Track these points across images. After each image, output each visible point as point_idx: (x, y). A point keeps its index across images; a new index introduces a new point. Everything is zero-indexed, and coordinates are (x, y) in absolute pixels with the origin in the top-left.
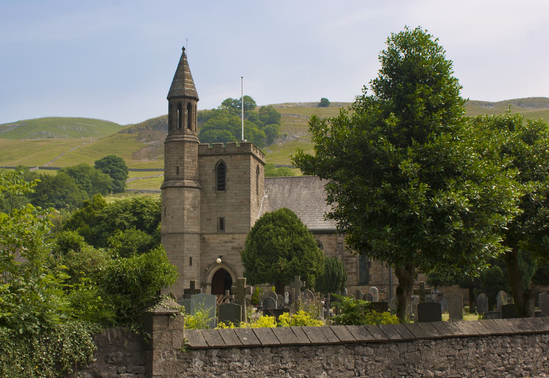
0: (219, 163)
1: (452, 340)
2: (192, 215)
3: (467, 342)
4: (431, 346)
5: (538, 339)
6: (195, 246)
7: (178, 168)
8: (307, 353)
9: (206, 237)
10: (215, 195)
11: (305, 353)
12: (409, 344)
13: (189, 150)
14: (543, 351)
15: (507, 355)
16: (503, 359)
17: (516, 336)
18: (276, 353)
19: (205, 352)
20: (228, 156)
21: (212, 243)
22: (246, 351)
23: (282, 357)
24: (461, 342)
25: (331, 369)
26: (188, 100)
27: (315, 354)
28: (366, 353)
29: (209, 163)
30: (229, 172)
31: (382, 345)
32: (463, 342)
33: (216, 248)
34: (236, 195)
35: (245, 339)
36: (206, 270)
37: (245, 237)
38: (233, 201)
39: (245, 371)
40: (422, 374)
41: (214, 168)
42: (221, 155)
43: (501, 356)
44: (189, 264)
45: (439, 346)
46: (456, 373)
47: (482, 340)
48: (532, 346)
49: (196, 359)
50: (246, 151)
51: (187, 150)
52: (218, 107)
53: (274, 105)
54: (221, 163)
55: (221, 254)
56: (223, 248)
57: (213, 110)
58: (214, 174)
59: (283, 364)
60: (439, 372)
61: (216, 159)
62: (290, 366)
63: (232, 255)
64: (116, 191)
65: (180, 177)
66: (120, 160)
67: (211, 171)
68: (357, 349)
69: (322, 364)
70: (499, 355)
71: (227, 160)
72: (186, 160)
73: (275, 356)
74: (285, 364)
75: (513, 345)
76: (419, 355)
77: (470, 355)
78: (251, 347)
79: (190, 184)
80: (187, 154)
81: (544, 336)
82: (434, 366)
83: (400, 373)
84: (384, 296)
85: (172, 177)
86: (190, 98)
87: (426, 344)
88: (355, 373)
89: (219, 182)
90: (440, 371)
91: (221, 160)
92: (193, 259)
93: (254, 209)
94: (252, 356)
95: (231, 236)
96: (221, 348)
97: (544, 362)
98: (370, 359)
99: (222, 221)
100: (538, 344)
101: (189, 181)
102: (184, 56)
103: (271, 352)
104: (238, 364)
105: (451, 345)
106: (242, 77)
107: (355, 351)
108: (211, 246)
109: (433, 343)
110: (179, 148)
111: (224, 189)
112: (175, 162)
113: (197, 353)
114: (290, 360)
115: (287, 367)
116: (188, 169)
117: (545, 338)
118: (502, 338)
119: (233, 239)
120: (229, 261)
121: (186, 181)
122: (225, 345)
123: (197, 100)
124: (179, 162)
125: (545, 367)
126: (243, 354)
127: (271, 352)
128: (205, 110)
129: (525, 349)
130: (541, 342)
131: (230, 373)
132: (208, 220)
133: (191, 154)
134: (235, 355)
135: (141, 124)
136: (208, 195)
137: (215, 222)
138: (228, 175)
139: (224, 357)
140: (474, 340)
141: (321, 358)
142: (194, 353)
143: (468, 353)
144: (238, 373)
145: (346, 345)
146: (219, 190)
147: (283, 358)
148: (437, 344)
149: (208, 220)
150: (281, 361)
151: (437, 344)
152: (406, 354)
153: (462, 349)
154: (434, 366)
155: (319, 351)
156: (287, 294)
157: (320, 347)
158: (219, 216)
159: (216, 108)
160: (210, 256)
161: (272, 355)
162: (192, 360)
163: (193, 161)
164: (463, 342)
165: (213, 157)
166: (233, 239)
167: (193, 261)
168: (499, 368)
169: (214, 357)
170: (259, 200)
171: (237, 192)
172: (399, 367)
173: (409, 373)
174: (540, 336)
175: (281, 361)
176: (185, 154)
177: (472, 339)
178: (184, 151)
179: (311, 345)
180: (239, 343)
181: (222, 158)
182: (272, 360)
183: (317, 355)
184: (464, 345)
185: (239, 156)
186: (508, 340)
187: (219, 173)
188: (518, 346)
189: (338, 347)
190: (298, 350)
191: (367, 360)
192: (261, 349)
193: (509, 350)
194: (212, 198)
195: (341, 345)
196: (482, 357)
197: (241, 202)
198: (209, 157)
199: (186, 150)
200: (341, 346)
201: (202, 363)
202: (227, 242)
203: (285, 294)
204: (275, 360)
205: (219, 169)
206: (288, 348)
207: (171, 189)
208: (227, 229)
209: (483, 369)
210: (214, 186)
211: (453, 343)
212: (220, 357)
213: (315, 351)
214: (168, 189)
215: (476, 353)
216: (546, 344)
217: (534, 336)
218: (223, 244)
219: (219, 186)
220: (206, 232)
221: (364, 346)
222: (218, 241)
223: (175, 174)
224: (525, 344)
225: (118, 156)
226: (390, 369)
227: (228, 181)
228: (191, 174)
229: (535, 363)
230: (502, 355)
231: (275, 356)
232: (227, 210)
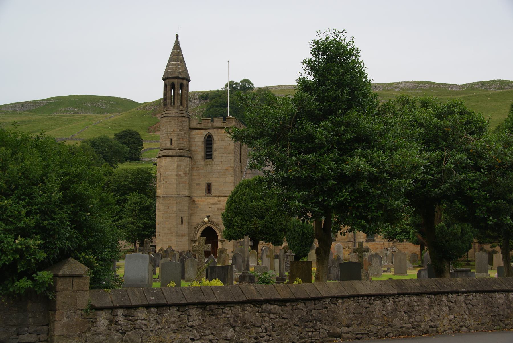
1: (359, 299)
3: (374, 301)
4: (338, 304)
5: (444, 298)
7: (171, 139)
8: (214, 311)
9: (196, 199)
10: (203, 163)
11: (212, 311)
12: (317, 302)
14: (450, 310)
15: (414, 313)
16: (410, 317)
17: (423, 295)
18: (183, 311)
19: (110, 311)
20: (215, 130)
22: (152, 309)
23: (189, 315)
24: (368, 300)
25: (238, 326)
27: (223, 312)
28: (272, 311)
29: (199, 136)
30: (216, 144)
31: (289, 303)
32: (370, 300)
33: (204, 209)
34: (221, 164)
35: (152, 298)
36: (195, 228)
37: (226, 199)
38: (219, 168)
39: (151, 329)
40: (328, 330)
42: (209, 129)
43: (408, 314)
44: (180, 223)
45: (346, 304)
46: (363, 329)
47: (389, 299)
48: (439, 304)
49: (101, 319)
52: (222, 88)
53: (269, 87)
54: (209, 135)
55: (208, 215)
56: (210, 209)
57: (218, 91)
58: (203, 145)
59: (190, 321)
60: (346, 328)
61: (205, 132)
62: (197, 323)
64: (132, 159)
66: (136, 133)
67: (201, 143)
68: (264, 307)
69: (229, 321)
70: (405, 313)
73: (181, 315)
74: (192, 321)
75: (419, 303)
76: (326, 313)
77: (376, 312)
78: (157, 306)
79: (182, 153)
81: (450, 295)
82: (341, 323)
83: (307, 329)
84: (349, 251)
85: (166, 147)
86: (183, 79)
87: (334, 302)
88: (262, 330)
89: (207, 152)
90: (347, 327)
92: (184, 218)
93: (238, 176)
94: (159, 314)
96: (127, 308)
97: (450, 320)
98: (278, 317)
99: (209, 186)
100: (445, 303)
102: (177, 42)
103: (178, 310)
104: (144, 322)
105: (358, 303)
106: (228, 61)
107: (262, 309)
109: (340, 301)
110: (173, 122)
112: (169, 135)
113: (102, 313)
114: (197, 318)
115: (194, 325)
117: (452, 297)
118: (409, 297)
120: (215, 221)
122: (130, 304)
123: (189, 80)
124: (172, 135)
125: (452, 324)
126: (149, 312)
127: (178, 310)
128: (210, 91)
129: (431, 307)
130: (447, 301)
131: (136, 331)
132: (197, 184)
133: (183, 128)
134: (141, 314)
135: (152, 102)
137: (204, 186)
138: (215, 146)
139: (130, 316)
140: (381, 298)
141: (228, 316)
142: (100, 312)
143: (375, 311)
144: (144, 331)
145: (253, 303)
146: (207, 159)
147: (190, 316)
148: (343, 302)
149: (197, 184)
150: (188, 319)
151: (343, 302)
152: (313, 311)
153: (369, 307)
154: (341, 323)
155: (227, 308)
157: (227, 305)
159: (220, 89)
160: (198, 216)
161: (179, 313)
162: (96, 319)
163: (185, 134)
164: (370, 300)
165: (202, 131)
167: (184, 221)
168: (405, 325)
169: (120, 316)
170: (243, 168)
171: (222, 160)
172: (306, 323)
173: (315, 330)
174: (447, 295)
175: (188, 319)
177: (379, 298)
179: (219, 304)
180: (145, 303)
181: (210, 131)
182: (179, 318)
183: (224, 313)
184: (371, 303)
186: (415, 298)
187: (207, 144)
188: (425, 305)
189: (246, 305)
190: (205, 309)
191: (274, 318)
192: (168, 307)
193: (416, 309)
194: (201, 166)
195: (249, 303)
196: (389, 315)
197: (226, 169)
198: (198, 131)
200: (249, 305)
201: (106, 322)
202: (213, 204)
204: (182, 317)
205: (207, 141)
206: (196, 307)
207: (164, 157)
208: (214, 192)
209: (390, 325)
210: (203, 155)
211: (360, 301)
212: (126, 316)
213: (222, 309)
214: (163, 158)
215: (383, 310)
216: (452, 302)
217: (441, 295)
218: (210, 206)
219: (207, 155)
220: (196, 195)
221: (271, 304)
222: (206, 203)
223: (169, 145)
224: (432, 303)
225: (134, 129)
226: (297, 326)
227: (215, 151)
228: (183, 145)
229: (442, 320)
230: (409, 313)
231: (181, 315)
232: (214, 176)
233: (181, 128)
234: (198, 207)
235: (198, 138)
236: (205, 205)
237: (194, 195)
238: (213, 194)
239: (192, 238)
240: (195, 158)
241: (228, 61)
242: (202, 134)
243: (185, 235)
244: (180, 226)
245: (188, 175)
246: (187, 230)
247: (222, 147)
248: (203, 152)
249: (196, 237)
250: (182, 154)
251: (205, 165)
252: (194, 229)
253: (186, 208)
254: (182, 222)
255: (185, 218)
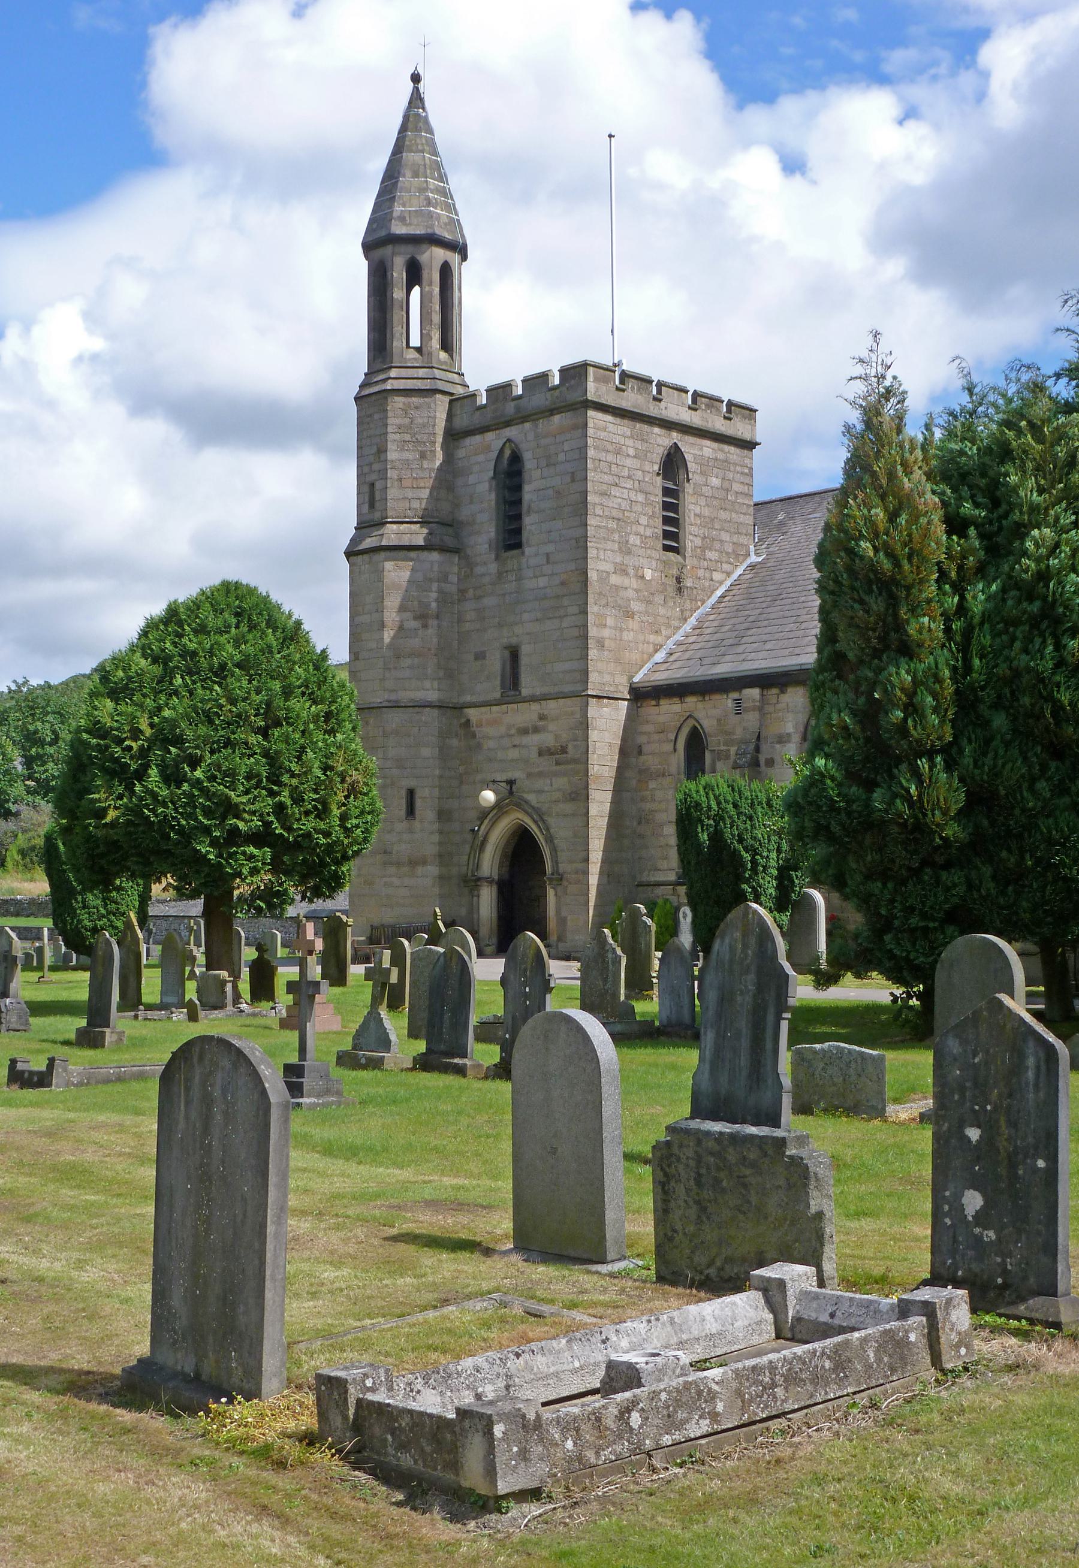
0: (507, 453)
2: (415, 643)
6: (426, 752)
9: (472, 713)
10: (493, 568)
13: (407, 421)
21: (489, 738)
26: (408, 250)
30: (530, 483)
33: (500, 755)
38: (542, 582)
41: (491, 473)
42: (508, 424)
44: (403, 813)
50: (575, 397)
51: (398, 421)
56: (514, 754)
58: (493, 496)
63: (540, 774)
65: (377, 515)
67: (486, 486)
71: (694, 450)
72: (392, 455)
80: (397, 437)
91: (509, 440)
92: (418, 794)
95: (535, 706)
101: (403, 527)
102: (416, 100)
106: (610, 136)
108: (485, 747)
111: (518, 545)
116: (401, 487)
119: (542, 717)
121: (395, 526)
133: (414, 435)
136: (479, 570)
137: (495, 662)
138: (528, 493)
156: (685, 917)
158: (505, 640)
165: (490, 436)
166: (542, 717)
171: (550, 548)
176: (391, 437)
178: (386, 425)
181: (511, 432)
185: (556, 419)
199: (393, 422)
202: (524, 731)
203: (681, 915)
208: (528, 685)
210: (493, 535)
218: (517, 741)
222: (502, 730)
232: (526, 616)
233: (407, 437)
234: (479, 746)
235: (476, 468)
236: (502, 737)
237: (468, 698)
238: (525, 692)
239: (464, 869)
240: (469, 551)
241: (610, 136)
242: (488, 449)
243: (424, 862)
244: (401, 826)
245: (433, 622)
246: (436, 838)
247: (550, 492)
248: (494, 523)
249: (478, 867)
250: (406, 541)
251: (500, 574)
252: (469, 837)
253: (426, 752)
254: (411, 811)
255: (426, 792)
